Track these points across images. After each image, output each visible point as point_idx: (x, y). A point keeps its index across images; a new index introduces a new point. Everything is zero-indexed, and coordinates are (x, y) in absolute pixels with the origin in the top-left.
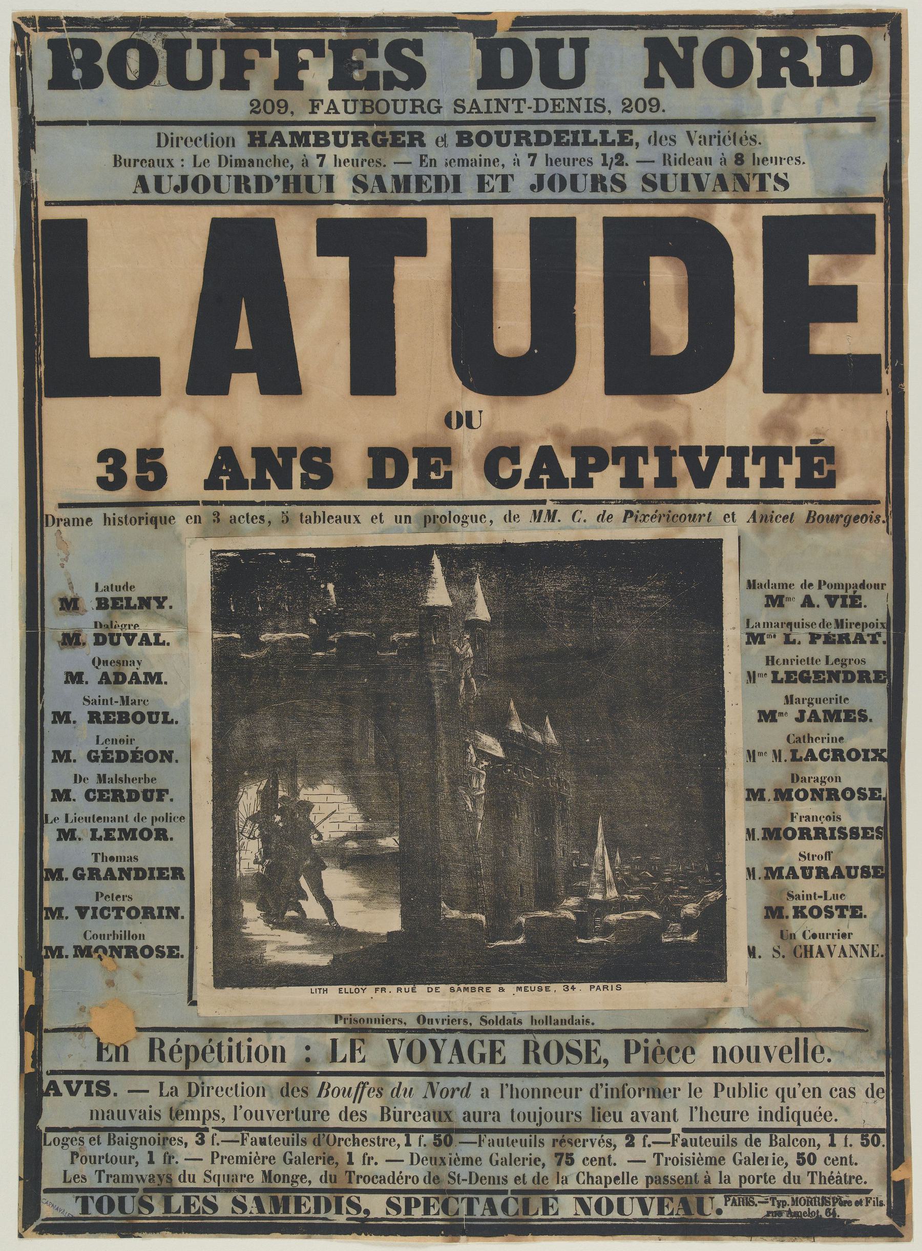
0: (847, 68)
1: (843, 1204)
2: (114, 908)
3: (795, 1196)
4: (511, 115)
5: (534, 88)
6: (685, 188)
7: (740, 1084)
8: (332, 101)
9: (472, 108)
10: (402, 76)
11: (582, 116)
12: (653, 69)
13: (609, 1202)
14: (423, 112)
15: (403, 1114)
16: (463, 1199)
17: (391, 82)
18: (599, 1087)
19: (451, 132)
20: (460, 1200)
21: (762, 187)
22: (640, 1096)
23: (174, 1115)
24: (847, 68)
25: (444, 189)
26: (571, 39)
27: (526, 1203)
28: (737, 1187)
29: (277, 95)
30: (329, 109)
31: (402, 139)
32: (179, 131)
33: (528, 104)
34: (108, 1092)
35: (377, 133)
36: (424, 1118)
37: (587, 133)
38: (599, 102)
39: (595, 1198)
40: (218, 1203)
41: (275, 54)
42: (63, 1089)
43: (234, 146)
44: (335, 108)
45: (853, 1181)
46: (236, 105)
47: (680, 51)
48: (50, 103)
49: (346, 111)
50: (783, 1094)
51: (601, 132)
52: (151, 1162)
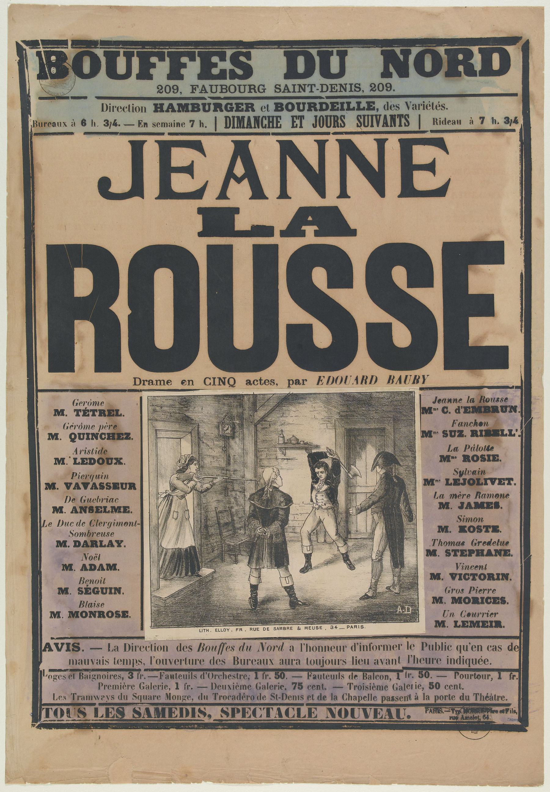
0: (496, 64)
2: (471, 574)
4: (307, 94)
5: (316, 78)
8: (203, 86)
9: (285, 89)
10: (239, 72)
11: (348, 94)
12: (386, 67)
13: (187, 711)
14: (255, 92)
15: (246, 661)
16: (264, 708)
17: (234, 75)
18: (356, 645)
19: (271, 104)
20: (262, 709)
23: (116, 662)
24: (496, 64)
27: (299, 710)
28: (433, 702)
29: (172, 83)
30: (202, 90)
31: (242, 107)
32: (114, 103)
33: (317, 87)
35: (228, 104)
36: (258, 663)
37: (349, 103)
38: (357, 85)
42: (53, 647)
43: (145, 112)
44: (205, 90)
45: (500, 699)
46: (148, 88)
47: (401, 57)
49: (212, 92)
50: (460, 649)
51: (357, 102)
52: (177, 688)
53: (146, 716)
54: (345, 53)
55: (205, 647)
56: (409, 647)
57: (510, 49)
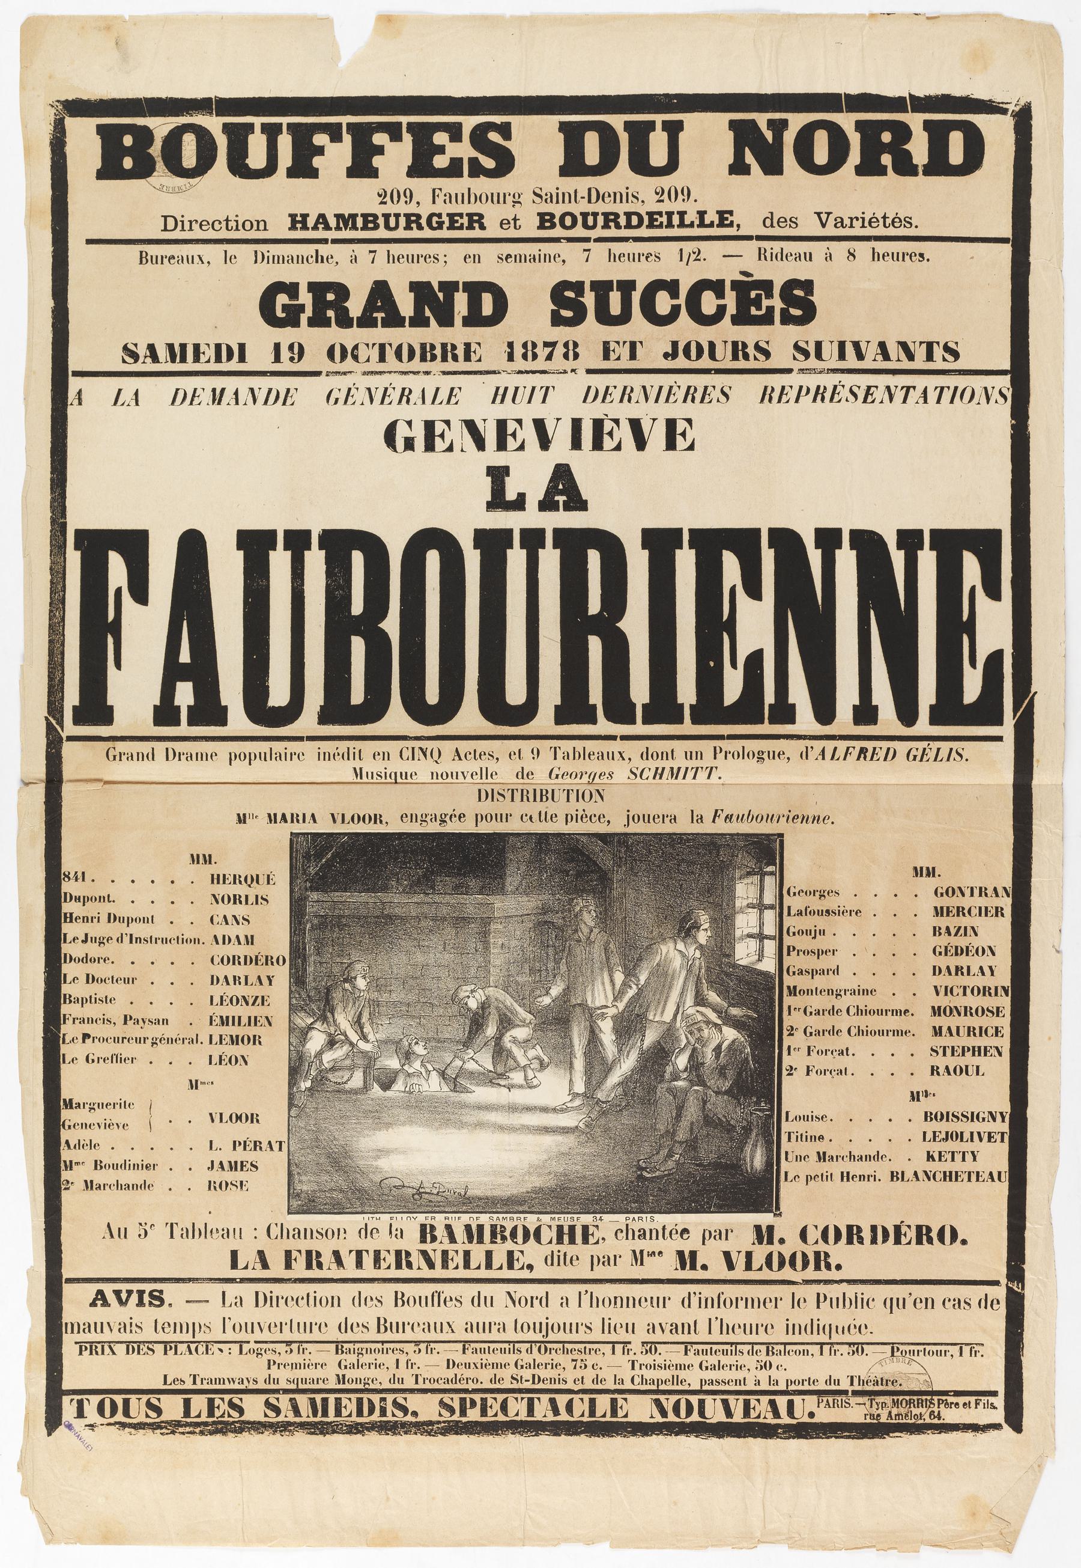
0: (956, 155)
1: (948, 1405)
3: (895, 1398)
5: (622, 176)
6: (842, 356)
10: (489, 163)
12: (739, 155)
16: (522, 1399)
17: (477, 169)
18: (692, 1295)
21: (930, 357)
24: (956, 155)
34: (162, 1301)
41: (347, 138)
42: (111, 1298)
45: (890, 1383)
47: (769, 136)
48: (95, 203)
53: (291, 1414)
55: (405, 1299)
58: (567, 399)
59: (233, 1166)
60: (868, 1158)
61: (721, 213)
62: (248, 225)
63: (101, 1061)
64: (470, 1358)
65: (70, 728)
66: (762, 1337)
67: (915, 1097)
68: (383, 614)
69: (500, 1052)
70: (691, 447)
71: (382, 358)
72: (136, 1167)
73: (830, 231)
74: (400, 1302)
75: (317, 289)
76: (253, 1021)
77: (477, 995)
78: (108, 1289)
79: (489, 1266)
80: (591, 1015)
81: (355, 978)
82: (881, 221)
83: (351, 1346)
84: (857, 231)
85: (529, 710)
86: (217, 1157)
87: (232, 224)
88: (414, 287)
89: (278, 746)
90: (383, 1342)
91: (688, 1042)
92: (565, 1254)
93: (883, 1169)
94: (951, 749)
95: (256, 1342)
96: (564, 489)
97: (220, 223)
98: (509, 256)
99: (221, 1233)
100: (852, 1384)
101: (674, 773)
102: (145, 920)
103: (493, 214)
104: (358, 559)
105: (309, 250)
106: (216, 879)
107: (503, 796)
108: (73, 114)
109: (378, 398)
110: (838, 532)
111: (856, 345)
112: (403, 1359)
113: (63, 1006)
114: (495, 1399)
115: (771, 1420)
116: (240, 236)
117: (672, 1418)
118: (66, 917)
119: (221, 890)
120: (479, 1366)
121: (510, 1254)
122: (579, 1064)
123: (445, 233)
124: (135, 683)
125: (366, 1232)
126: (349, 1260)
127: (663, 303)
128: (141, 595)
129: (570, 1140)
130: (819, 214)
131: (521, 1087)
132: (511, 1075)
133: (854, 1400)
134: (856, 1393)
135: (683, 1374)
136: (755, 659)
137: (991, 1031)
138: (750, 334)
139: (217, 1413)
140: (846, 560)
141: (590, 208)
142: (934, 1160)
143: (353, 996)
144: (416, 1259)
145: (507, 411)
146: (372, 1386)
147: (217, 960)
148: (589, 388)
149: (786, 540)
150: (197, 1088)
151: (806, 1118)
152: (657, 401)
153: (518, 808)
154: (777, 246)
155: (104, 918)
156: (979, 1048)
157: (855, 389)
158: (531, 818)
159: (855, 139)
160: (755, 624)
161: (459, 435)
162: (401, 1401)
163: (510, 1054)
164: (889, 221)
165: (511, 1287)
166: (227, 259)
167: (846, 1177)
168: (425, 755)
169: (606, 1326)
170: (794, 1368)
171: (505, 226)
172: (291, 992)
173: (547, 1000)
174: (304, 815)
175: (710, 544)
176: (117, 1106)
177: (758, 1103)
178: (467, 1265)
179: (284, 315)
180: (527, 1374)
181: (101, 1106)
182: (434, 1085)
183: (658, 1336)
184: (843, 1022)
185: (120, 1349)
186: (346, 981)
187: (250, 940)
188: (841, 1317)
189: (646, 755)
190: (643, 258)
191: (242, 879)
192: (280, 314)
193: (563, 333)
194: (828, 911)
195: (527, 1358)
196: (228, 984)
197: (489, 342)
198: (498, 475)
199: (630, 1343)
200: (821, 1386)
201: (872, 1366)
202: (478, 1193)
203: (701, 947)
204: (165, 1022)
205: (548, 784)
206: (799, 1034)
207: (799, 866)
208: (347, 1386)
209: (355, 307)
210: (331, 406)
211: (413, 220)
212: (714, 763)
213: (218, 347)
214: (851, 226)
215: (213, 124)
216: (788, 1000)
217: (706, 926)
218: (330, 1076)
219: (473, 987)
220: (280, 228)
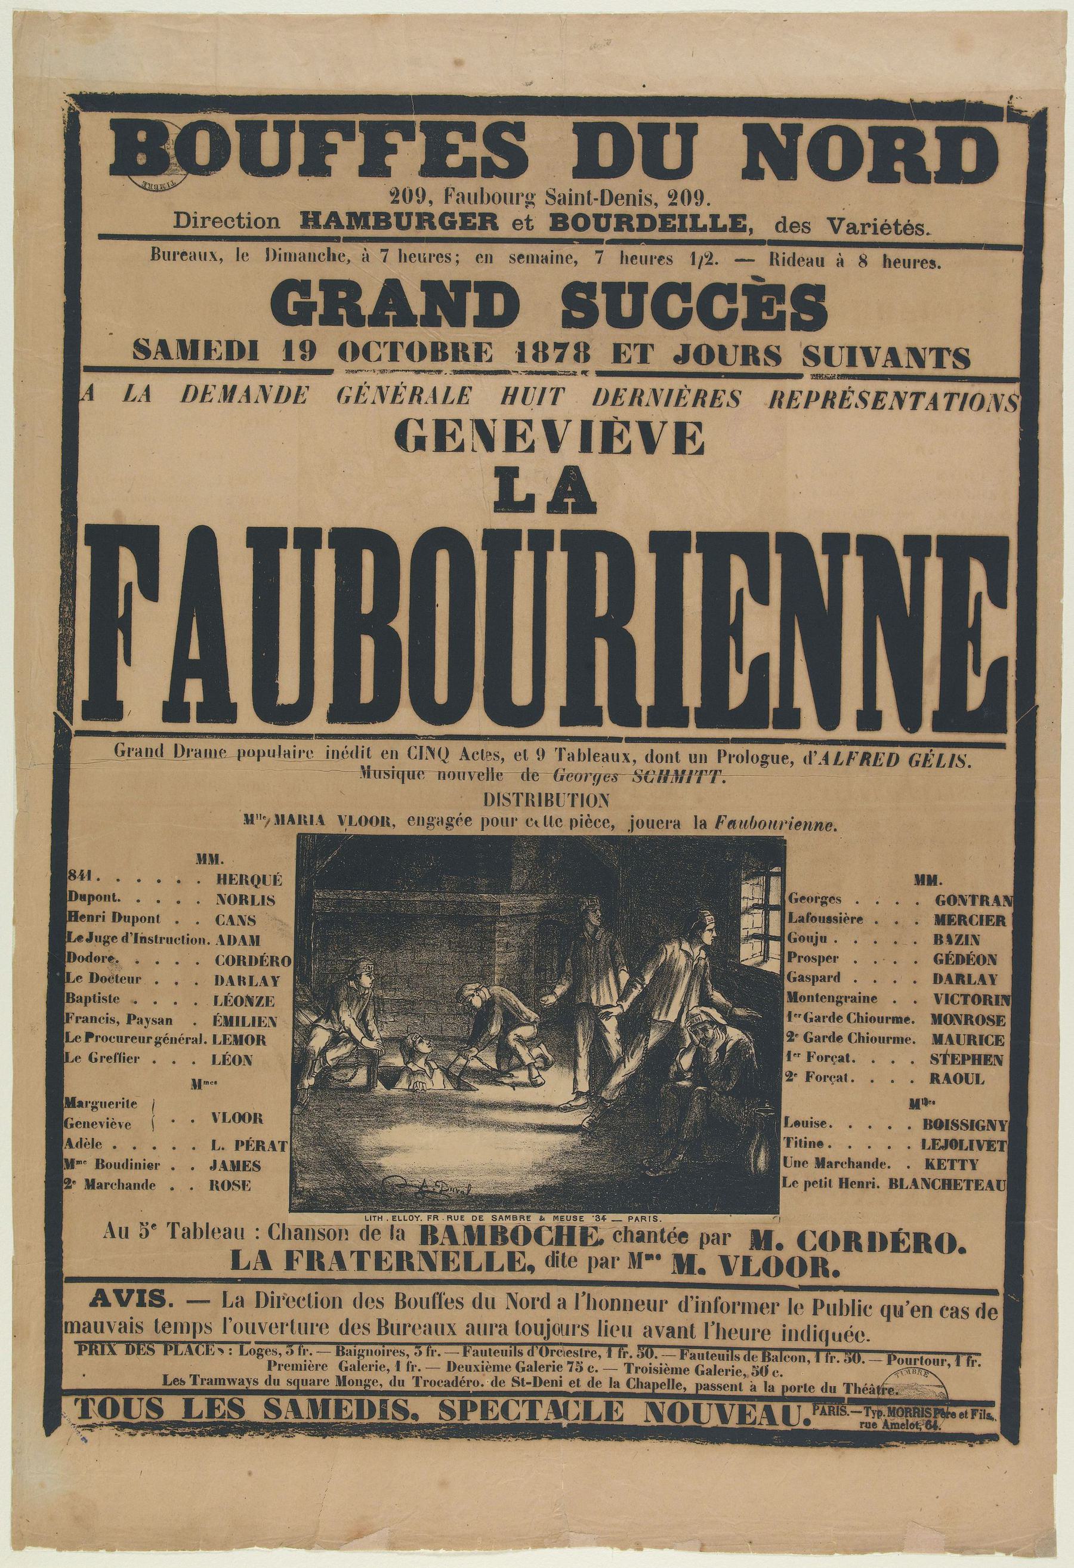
1: (945, 1415)
6: (852, 362)
7: (841, 1300)
10: (501, 163)
13: (371, 1405)
16: (524, 1402)
17: (490, 170)
18: (689, 1299)
21: (939, 364)
22: (734, 1312)
25: (236, 356)
26: (276, 123)
27: (588, 1406)
34: (163, 1302)
39: (669, 1402)
40: (164, 1406)
41: (360, 137)
47: (783, 140)
53: (291, 1415)
54: (693, 129)
56: (793, 1309)
57: (998, 130)
58: (576, 400)
59: (236, 1166)
60: (867, 1165)
61: (734, 218)
62: (260, 223)
63: (104, 1060)
64: (471, 1360)
65: (78, 723)
66: (759, 1343)
67: (914, 1104)
68: (393, 612)
69: (505, 1052)
70: (700, 451)
71: (394, 357)
72: (138, 1166)
73: (843, 236)
74: (401, 1304)
75: (329, 287)
76: (258, 1022)
77: (481, 994)
78: (109, 1288)
79: (490, 1267)
80: (597, 1014)
81: (360, 975)
82: (893, 227)
83: (351, 1347)
84: (869, 237)
85: (534, 711)
86: (220, 1157)
87: (245, 221)
88: (426, 285)
89: (287, 745)
90: (383, 1344)
91: (693, 1041)
92: (564, 1255)
93: (882, 1177)
94: (954, 755)
95: (256, 1343)
96: (572, 491)
97: (233, 220)
98: (521, 256)
99: (223, 1232)
100: (848, 1392)
101: (679, 777)
102: (151, 920)
103: (506, 215)
104: (368, 558)
105: (321, 248)
106: (221, 879)
107: (509, 800)
108: (85, 109)
109: (389, 397)
110: (846, 536)
111: (866, 351)
112: (404, 1361)
113: (66, 1004)
114: (496, 1402)
115: (765, 1425)
116: (251, 233)
117: (667, 1421)
118: (70, 916)
119: (228, 890)
120: (480, 1368)
121: (511, 1255)
122: (583, 1063)
123: (457, 233)
124: (144, 681)
125: (368, 1234)
126: (351, 1262)
127: (675, 306)
128: (151, 592)
129: (575, 1138)
130: (831, 220)
131: (525, 1085)
132: (515, 1073)
133: (850, 1408)
134: (853, 1401)
135: (678, 1378)
136: (761, 662)
137: (991, 1040)
138: (760, 339)
139: (218, 1414)
140: (853, 566)
141: (604, 210)
142: (933, 1168)
143: (355, 996)
144: (417, 1260)
145: (517, 411)
146: (373, 1388)
147: (222, 960)
148: (600, 390)
149: (793, 545)
150: (200, 1088)
151: (805, 1124)
152: (666, 404)
153: (521, 813)
154: (789, 251)
155: (109, 917)
156: (980, 1056)
157: (865, 395)
158: (536, 822)
159: (868, 145)
160: (761, 629)
161: (468, 434)
162: (401, 1403)
163: (514, 1052)
164: (900, 228)
165: (513, 1289)
166: (240, 256)
167: (844, 1183)
168: (433, 755)
169: (604, 1329)
170: (791, 1374)
171: (518, 227)
172: (295, 989)
173: (552, 999)
174: (312, 816)
175: (718, 547)
176: (120, 1106)
177: (762, 1104)
178: (468, 1267)
179: (295, 313)
180: (528, 1376)
181: (104, 1105)
182: (437, 1083)
183: (655, 1340)
184: (843, 1029)
185: (120, 1349)
186: (350, 979)
187: (255, 941)
188: (838, 1324)
189: (651, 757)
190: (655, 261)
191: (249, 879)
192: (291, 311)
193: (574, 335)
194: (829, 918)
195: (529, 1361)
196: (232, 984)
197: (502, 342)
198: (507, 476)
199: (626, 1346)
200: (818, 1393)
201: (872, 1373)
202: (482, 1191)
203: (705, 947)
204: (169, 1021)
205: (554, 787)
206: (799, 1040)
207: (803, 871)
208: (348, 1388)
209: (367, 304)
210: (341, 406)
211: (425, 219)
212: (718, 766)
213: (230, 344)
214: (864, 233)
215: (227, 121)
216: (788, 1007)
217: (712, 926)
218: (334, 1074)
219: (477, 985)
220: (291, 226)
